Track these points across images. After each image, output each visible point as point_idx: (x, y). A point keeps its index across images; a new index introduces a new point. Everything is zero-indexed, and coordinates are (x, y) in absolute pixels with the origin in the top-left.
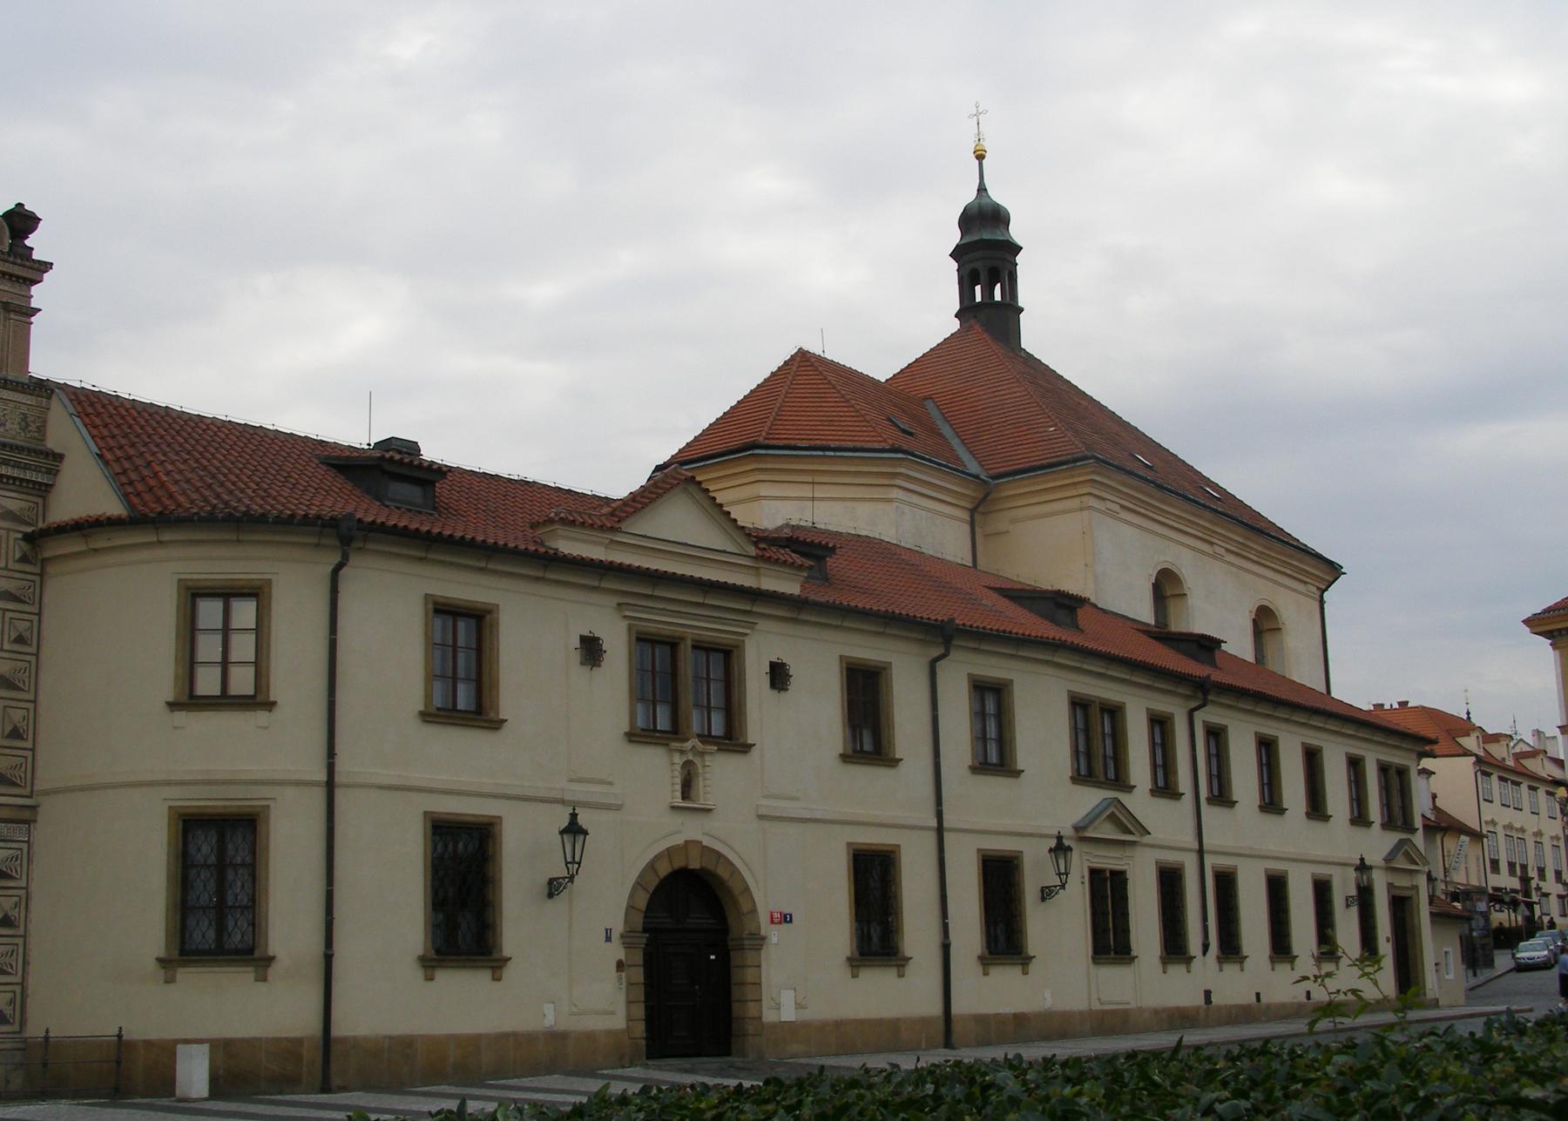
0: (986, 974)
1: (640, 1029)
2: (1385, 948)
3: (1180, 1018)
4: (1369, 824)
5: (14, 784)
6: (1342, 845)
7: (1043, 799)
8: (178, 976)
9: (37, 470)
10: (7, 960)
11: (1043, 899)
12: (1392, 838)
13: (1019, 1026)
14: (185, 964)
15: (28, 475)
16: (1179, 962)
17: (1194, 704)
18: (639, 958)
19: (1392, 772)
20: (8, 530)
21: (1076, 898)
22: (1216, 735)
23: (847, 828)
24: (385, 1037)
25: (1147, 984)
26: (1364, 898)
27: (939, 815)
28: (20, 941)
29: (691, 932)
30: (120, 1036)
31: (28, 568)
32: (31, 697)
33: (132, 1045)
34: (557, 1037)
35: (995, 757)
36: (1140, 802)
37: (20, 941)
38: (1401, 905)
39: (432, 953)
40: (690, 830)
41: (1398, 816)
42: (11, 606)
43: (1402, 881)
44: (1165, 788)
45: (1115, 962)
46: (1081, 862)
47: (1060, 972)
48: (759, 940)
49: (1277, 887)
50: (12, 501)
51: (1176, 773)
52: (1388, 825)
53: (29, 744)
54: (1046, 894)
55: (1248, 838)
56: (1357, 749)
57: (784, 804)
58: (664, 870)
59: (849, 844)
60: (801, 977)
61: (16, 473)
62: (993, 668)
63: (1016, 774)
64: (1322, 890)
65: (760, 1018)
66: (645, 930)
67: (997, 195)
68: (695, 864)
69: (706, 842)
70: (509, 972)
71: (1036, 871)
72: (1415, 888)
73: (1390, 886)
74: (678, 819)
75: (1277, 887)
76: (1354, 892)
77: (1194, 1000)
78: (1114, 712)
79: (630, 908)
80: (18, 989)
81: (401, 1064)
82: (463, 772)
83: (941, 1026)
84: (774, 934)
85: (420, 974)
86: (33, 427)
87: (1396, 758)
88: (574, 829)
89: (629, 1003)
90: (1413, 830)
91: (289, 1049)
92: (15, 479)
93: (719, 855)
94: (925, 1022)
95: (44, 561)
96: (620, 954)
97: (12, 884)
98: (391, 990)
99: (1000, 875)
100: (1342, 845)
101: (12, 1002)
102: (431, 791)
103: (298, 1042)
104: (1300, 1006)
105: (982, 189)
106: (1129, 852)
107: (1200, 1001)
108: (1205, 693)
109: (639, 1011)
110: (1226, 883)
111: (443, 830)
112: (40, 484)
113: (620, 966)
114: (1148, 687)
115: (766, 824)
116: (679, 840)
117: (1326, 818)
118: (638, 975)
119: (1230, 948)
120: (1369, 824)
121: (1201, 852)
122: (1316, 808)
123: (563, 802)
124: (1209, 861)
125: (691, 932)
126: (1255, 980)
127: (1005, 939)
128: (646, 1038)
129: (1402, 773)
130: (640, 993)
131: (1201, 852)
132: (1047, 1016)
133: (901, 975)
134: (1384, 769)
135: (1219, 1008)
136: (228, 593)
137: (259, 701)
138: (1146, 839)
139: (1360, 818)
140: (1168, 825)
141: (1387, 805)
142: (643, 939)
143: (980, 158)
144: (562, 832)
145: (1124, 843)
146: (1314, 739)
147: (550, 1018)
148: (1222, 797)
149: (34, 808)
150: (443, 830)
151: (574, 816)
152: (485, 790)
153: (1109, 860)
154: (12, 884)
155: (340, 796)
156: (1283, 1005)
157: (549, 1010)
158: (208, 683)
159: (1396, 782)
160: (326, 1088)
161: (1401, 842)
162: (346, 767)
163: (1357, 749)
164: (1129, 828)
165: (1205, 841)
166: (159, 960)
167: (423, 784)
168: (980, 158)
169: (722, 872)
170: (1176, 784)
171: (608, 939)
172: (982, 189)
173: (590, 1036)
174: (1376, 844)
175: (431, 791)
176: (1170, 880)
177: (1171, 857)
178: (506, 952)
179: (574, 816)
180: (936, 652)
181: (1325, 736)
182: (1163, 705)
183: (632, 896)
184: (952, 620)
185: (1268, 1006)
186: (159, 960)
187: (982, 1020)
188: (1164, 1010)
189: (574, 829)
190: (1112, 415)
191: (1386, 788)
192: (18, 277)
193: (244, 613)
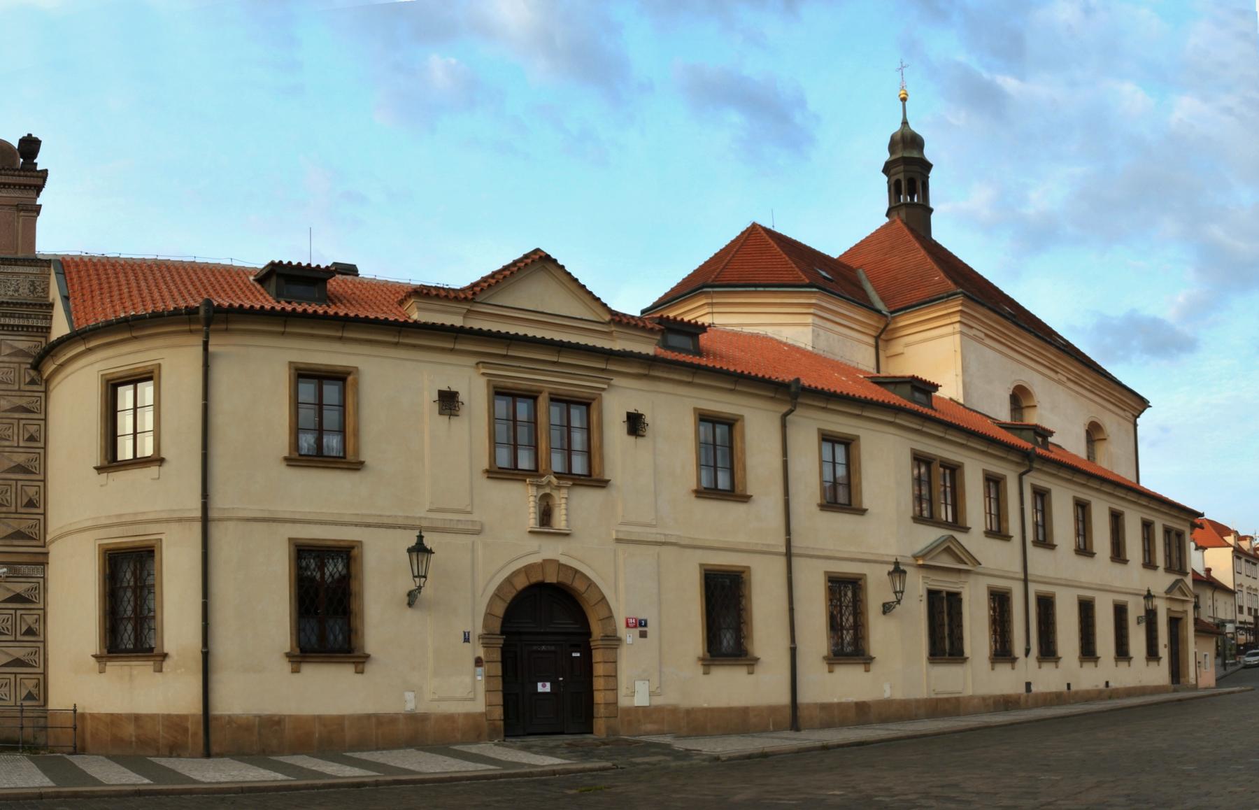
0: (831, 671)
1: (498, 713)
2: (1164, 652)
3: (1006, 703)
4: (1155, 568)
5: (31, 538)
6: (1136, 580)
7: (885, 529)
8: (108, 668)
9: (37, 317)
10: (32, 657)
11: (884, 613)
12: (1172, 578)
13: (862, 712)
14: (110, 659)
15: (31, 322)
16: (148, 658)
17: (1023, 470)
18: (497, 655)
19: (1173, 534)
20: (20, 363)
21: (916, 609)
22: (1041, 495)
23: (699, 552)
24: (255, 716)
25: (977, 677)
26: (1150, 618)
27: (788, 543)
28: (41, 645)
29: (546, 635)
30: (75, 711)
31: (35, 388)
32: (41, 477)
33: (83, 715)
34: (415, 719)
35: (841, 497)
36: (975, 541)
37: (41, 645)
38: (1175, 623)
39: (297, 651)
40: (551, 550)
41: (1177, 564)
42: (23, 416)
43: (1177, 607)
44: (998, 532)
45: (948, 662)
46: (917, 585)
47: (899, 666)
48: (613, 641)
49: (1086, 609)
50: (23, 343)
51: (1007, 521)
52: (1169, 569)
53: (41, 511)
54: (887, 608)
55: (1063, 571)
56: (1149, 516)
57: (639, 533)
58: (521, 583)
59: (701, 565)
60: (653, 670)
61: (21, 322)
62: (841, 425)
63: (862, 512)
64: (1120, 611)
65: (616, 703)
66: (502, 633)
67: (915, 127)
68: (551, 578)
69: (563, 560)
70: (1061, 664)
71: (877, 592)
72: (1185, 612)
73: (1169, 610)
74: (535, 542)
75: (1086, 609)
76: (1143, 613)
77: (1017, 689)
78: (954, 470)
79: (489, 615)
80: (41, 677)
81: (264, 738)
82: (324, 504)
83: (788, 712)
84: (629, 637)
85: (287, 666)
86: (39, 289)
87: (1176, 525)
88: (420, 549)
89: (488, 691)
90: (1186, 574)
91: (175, 723)
92: (23, 326)
93: (576, 571)
94: (773, 710)
95: (47, 381)
96: (481, 652)
97: (32, 606)
98: (265, 680)
99: (845, 593)
100: (1136, 580)
101: (37, 685)
102: (294, 521)
103: (183, 718)
104: (1100, 692)
105: (905, 123)
106: (963, 577)
107: (1022, 690)
108: (1031, 461)
109: (498, 698)
110: (1046, 605)
111: (308, 556)
112: (42, 328)
113: (478, 662)
114: (983, 452)
115: (622, 546)
116: (537, 559)
117: (1125, 562)
118: (497, 669)
119: (1048, 651)
120: (1155, 568)
121: (1026, 581)
122: (1118, 554)
123: (412, 528)
124: (1033, 588)
125: (546, 635)
126: (1068, 673)
127: (849, 646)
128: (505, 720)
129: (1180, 535)
130: (498, 684)
131: (1026, 581)
132: (889, 703)
133: (751, 673)
134: (1167, 531)
135: (1037, 695)
136: (135, 379)
137: (157, 460)
138: (979, 569)
139: (1149, 564)
140: (999, 559)
141: (1168, 556)
142: (500, 641)
143: (904, 100)
144: (410, 551)
145: (959, 571)
146: (1119, 506)
147: (409, 704)
148: (1045, 541)
149: (46, 554)
150: (308, 556)
151: (420, 537)
152: (346, 519)
153: (946, 584)
154: (32, 606)
155: (216, 531)
156: (1088, 692)
157: (409, 696)
158: (125, 452)
159: (1175, 542)
160: (208, 754)
161: (1177, 582)
162: (220, 502)
163: (1149, 516)
164: (965, 563)
165: (1029, 571)
166: (95, 656)
167: (287, 516)
168: (904, 100)
169: (579, 585)
170: (1007, 529)
171: (467, 640)
172: (905, 123)
173: (450, 718)
174: (1160, 581)
175: (294, 521)
176: (1000, 600)
177: (1000, 583)
178: (873, 654)
179: (420, 537)
180: (785, 409)
181: (1126, 504)
182: (997, 468)
183: (490, 605)
184: (798, 380)
185: (1076, 693)
186: (95, 656)
187: (825, 707)
188: (990, 697)
189: (420, 549)
190: (956, 258)
191: (1168, 545)
192: (25, 186)
193: (147, 390)
